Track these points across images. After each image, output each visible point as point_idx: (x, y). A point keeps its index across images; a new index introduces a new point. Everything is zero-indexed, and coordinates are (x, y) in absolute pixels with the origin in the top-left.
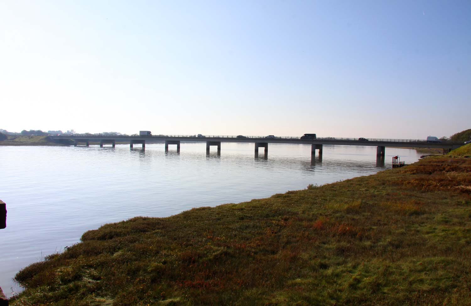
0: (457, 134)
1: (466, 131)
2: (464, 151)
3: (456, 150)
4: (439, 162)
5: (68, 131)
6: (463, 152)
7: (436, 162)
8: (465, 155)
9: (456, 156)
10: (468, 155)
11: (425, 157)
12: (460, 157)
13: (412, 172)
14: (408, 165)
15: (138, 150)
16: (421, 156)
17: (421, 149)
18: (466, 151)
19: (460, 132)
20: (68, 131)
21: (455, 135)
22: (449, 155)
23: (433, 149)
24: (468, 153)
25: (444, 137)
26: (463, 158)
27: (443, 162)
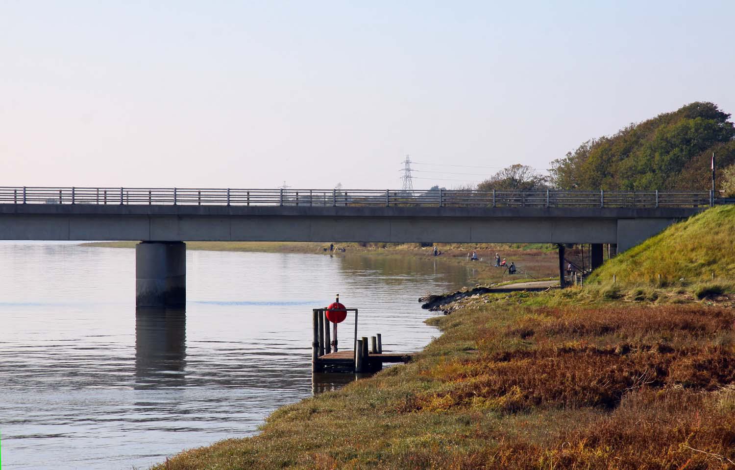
0: (597, 146)
1: (649, 125)
2: (693, 255)
3: (637, 249)
4: (579, 330)
5: (186, 341)
6: (683, 262)
7: (559, 331)
8: (698, 286)
9: (649, 291)
10: (718, 282)
11: (455, 305)
12: (672, 293)
13: (503, 400)
14: (406, 359)
15: (524, 289)
16: (425, 295)
17: (373, 252)
18: (700, 257)
19: (669, 112)
20: (186, 341)
21: (582, 154)
22: (606, 287)
23: (452, 248)
24: (714, 267)
25: (518, 167)
26: (690, 300)
27: (606, 330)
